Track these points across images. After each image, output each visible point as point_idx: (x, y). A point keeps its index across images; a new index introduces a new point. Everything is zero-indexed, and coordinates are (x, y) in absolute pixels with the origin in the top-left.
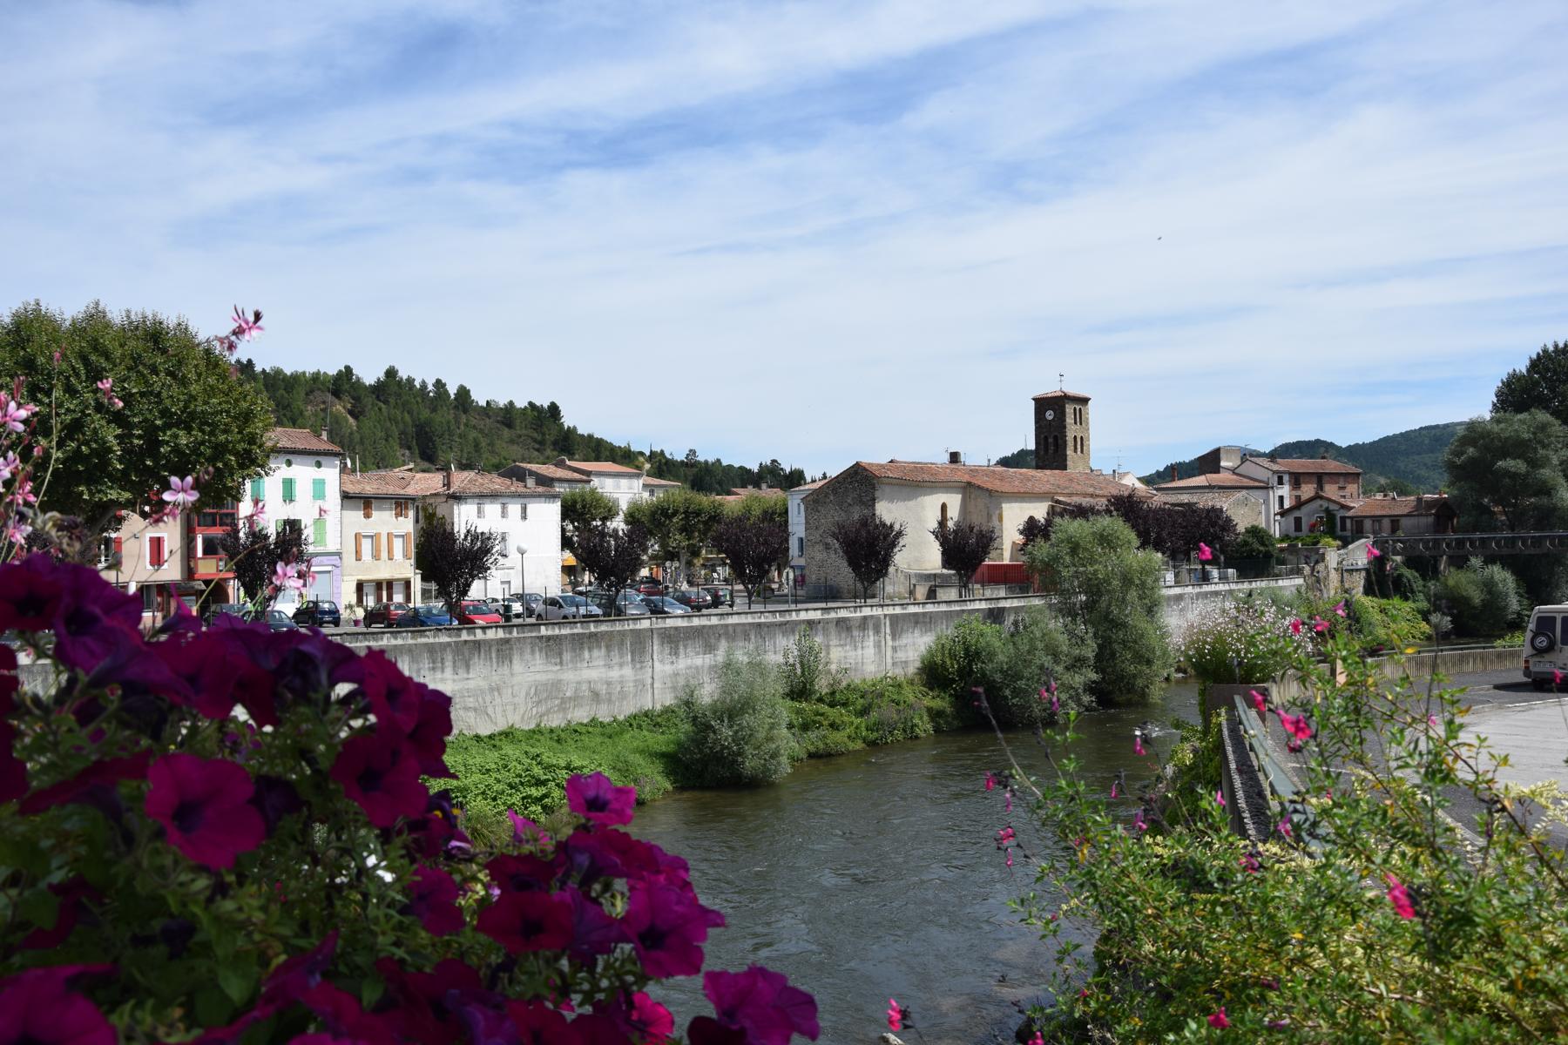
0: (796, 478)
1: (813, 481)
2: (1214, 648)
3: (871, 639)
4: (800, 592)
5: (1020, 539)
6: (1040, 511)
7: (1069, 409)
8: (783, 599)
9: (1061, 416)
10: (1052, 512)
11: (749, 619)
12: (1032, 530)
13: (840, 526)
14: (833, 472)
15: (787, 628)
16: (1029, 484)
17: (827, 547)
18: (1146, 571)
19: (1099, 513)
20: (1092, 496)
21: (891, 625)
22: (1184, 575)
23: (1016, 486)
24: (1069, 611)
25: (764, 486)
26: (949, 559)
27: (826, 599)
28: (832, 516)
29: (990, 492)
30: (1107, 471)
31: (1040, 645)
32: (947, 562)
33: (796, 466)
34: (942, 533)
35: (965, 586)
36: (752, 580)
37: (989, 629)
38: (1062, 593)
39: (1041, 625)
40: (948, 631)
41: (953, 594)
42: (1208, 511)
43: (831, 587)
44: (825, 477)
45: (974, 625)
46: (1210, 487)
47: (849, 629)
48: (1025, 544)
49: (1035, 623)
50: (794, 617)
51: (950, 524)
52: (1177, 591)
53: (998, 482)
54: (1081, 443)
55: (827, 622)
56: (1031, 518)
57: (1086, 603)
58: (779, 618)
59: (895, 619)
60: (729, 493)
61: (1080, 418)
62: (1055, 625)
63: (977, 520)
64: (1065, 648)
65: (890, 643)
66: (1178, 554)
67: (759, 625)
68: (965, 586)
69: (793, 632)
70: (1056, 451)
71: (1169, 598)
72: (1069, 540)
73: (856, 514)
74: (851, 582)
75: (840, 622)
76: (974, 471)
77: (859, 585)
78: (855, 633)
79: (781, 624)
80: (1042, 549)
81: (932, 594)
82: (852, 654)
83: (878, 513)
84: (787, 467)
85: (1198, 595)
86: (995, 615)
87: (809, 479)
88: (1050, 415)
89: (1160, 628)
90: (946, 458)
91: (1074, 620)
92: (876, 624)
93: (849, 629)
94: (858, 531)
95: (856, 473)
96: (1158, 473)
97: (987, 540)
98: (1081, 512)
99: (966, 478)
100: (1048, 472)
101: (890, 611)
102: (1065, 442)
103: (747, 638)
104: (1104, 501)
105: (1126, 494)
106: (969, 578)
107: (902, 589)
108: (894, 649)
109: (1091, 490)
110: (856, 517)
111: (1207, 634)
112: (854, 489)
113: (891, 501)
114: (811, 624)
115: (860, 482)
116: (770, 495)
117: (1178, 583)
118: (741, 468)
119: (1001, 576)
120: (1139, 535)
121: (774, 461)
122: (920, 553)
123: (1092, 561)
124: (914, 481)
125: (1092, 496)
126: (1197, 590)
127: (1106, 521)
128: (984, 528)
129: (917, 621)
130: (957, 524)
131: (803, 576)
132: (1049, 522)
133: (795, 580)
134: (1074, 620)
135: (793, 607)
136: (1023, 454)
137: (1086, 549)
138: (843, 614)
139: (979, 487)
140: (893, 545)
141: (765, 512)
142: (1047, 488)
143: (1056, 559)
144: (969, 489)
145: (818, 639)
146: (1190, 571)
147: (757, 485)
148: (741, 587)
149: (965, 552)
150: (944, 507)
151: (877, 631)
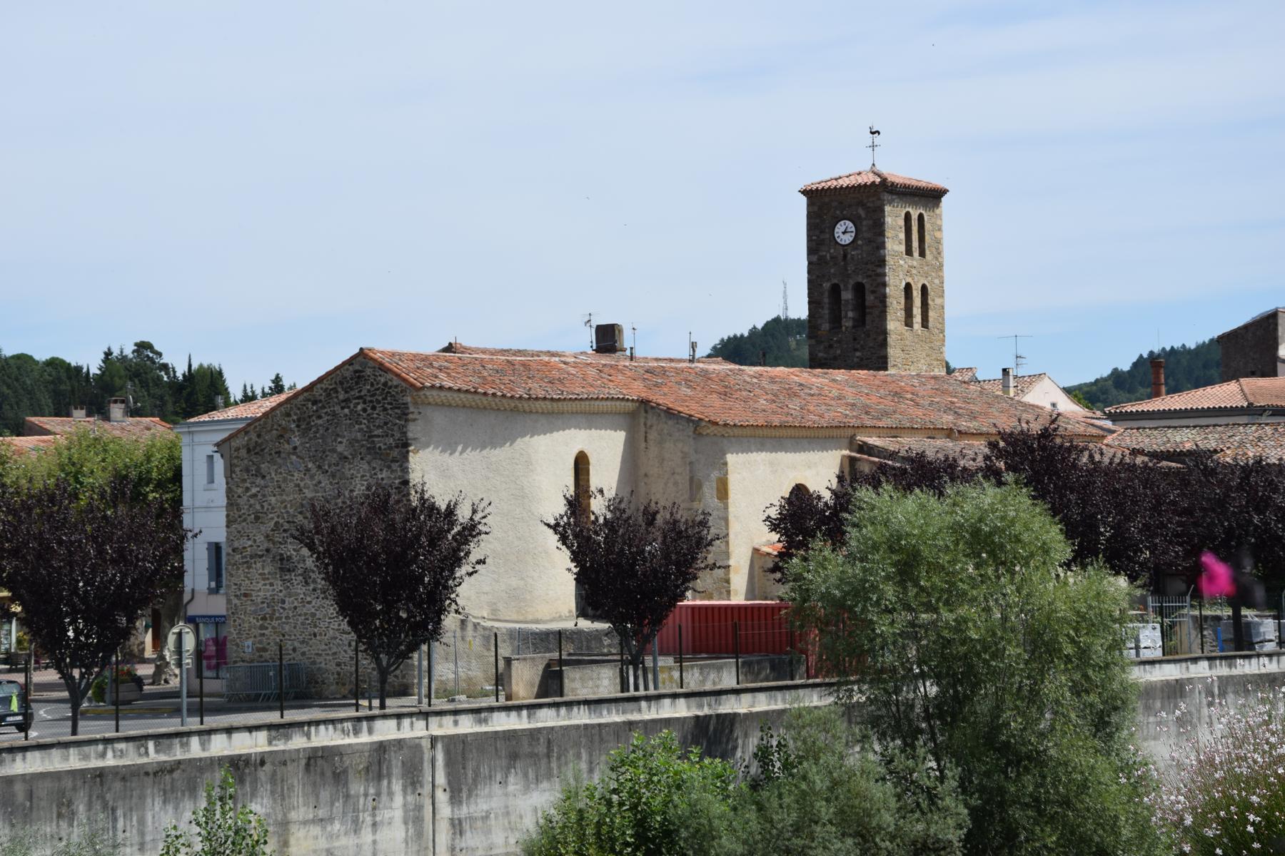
0: (202, 390)
1: (248, 398)
2: (1270, 822)
3: (396, 804)
4: (212, 685)
5: (770, 541)
6: (819, 472)
7: (894, 217)
8: (167, 704)
9: (873, 233)
10: (850, 476)
11: (74, 761)
12: (800, 518)
13: (319, 514)
14: (300, 376)
15: (174, 780)
16: (794, 405)
17: (285, 566)
18: (1092, 621)
19: (967, 476)
20: (949, 433)
21: (449, 763)
22: (1187, 634)
23: (762, 410)
24: (894, 723)
25: (117, 411)
26: (595, 592)
27: (280, 701)
28: (297, 487)
29: (696, 425)
30: (989, 371)
31: (825, 811)
32: (589, 603)
33: (202, 359)
34: (575, 528)
35: (636, 661)
36: (82, 654)
37: (696, 770)
38: (878, 677)
39: (828, 759)
40: (593, 776)
41: (604, 681)
42: (1247, 471)
43: (294, 670)
44: (278, 387)
45: (659, 760)
46: (1252, 412)
47: (339, 777)
48: (784, 555)
49: (812, 753)
50: (195, 749)
51: (598, 506)
52: (1171, 672)
53: (715, 401)
54: (922, 303)
55: (283, 760)
56: (799, 490)
57: (939, 701)
58: (153, 755)
59: (457, 749)
60: (21, 429)
61: (919, 240)
62: (862, 758)
63: (664, 494)
64: (888, 819)
65: (445, 810)
66: (1167, 583)
67: (100, 774)
68: (636, 661)
69: (192, 790)
70: (860, 321)
71: (1149, 692)
72: (894, 544)
73: (360, 481)
74: (346, 655)
75: (316, 759)
76: (656, 372)
77: (366, 663)
78: (357, 787)
79: (161, 771)
80: (827, 568)
81: (551, 684)
82: (347, 842)
83: (415, 477)
84: (178, 361)
85: (1224, 682)
86: (712, 735)
87: (236, 392)
88: (844, 232)
89: (1127, 768)
90: (586, 340)
91: (909, 746)
92: (410, 762)
93: (339, 777)
94: (364, 524)
95: (359, 377)
96: (1116, 375)
97: (690, 545)
98: (923, 474)
99: (637, 390)
100: (840, 375)
101: (444, 727)
102: (883, 299)
103: (64, 810)
104: (981, 446)
105: (1036, 428)
106: (646, 640)
107: (478, 671)
108: (457, 826)
109: (947, 420)
110: (360, 489)
111: (1252, 782)
112: (355, 418)
113: (449, 447)
114: (238, 765)
115: (368, 400)
116: (133, 433)
117: (1171, 653)
118: (54, 363)
119: (726, 635)
120: (1069, 533)
121: (143, 346)
122: (522, 581)
123: (952, 597)
124: (506, 399)
125: (949, 433)
126: (1222, 670)
127: (988, 495)
128: (683, 516)
129: (514, 750)
130: (616, 506)
131: (220, 643)
132: (843, 499)
133: (199, 654)
134: (909, 746)
135: (193, 723)
136: (778, 328)
137: (935, 567)
138: (325, 738)
139: (669, 413)
140: (455, 559)
141: (120, 479)
142: (837, 414)
143: (860, 591)
144: (642, 417)
145: (260, 807)
146: (1201, 622)
147: (98, 408)
148: (52, 676)
149: (634, 574)
150: (581, 464)
151: (413, 778)
